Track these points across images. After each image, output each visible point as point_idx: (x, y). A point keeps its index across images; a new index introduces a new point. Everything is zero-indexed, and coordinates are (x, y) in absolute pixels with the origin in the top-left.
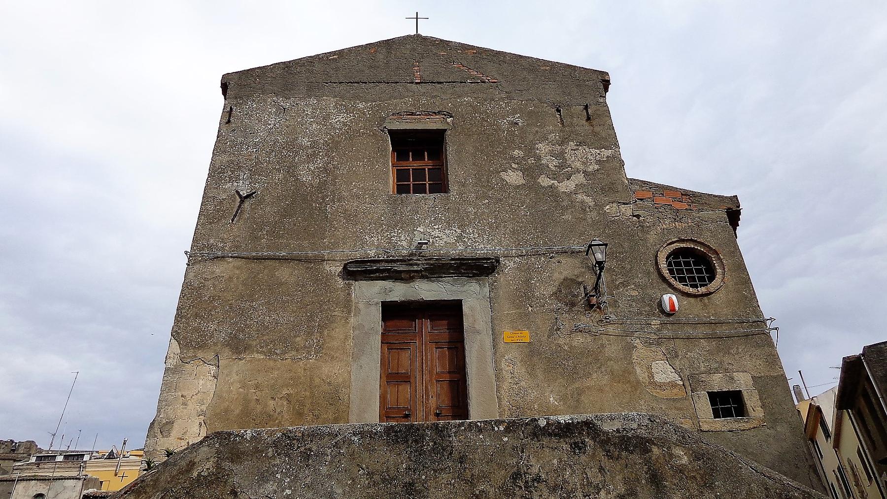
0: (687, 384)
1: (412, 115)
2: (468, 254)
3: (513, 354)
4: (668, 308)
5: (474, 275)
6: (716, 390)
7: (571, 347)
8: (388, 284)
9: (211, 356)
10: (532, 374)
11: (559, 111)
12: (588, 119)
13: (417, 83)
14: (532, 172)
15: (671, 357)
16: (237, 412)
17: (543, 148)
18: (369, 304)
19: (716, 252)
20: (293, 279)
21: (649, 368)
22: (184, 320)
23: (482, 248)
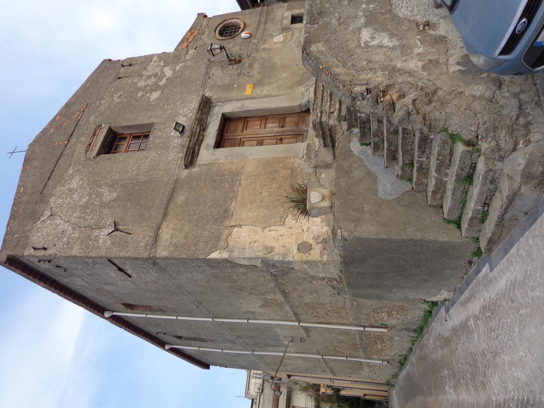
0: (286, 31)
1: (90, 145)
2: (126, 125)
3: (258, 91)
4: (249, 35)
5: (210, 107)
6: (290, 22)
7: (259, 69)
8: (203, 146)
9: (227, 232)
10: (270, 84)
11: (120, 78)
12: (131, 65)
13: (68, 143)
14: (155, 88)
15: (273, 36)
16: (265, 211)
17: (141, 84)
18: (213, 155)
19: (225, 21)
20: (186, 194)
21: (276, 43)
22: (197, 252)
23: (270, 232)
